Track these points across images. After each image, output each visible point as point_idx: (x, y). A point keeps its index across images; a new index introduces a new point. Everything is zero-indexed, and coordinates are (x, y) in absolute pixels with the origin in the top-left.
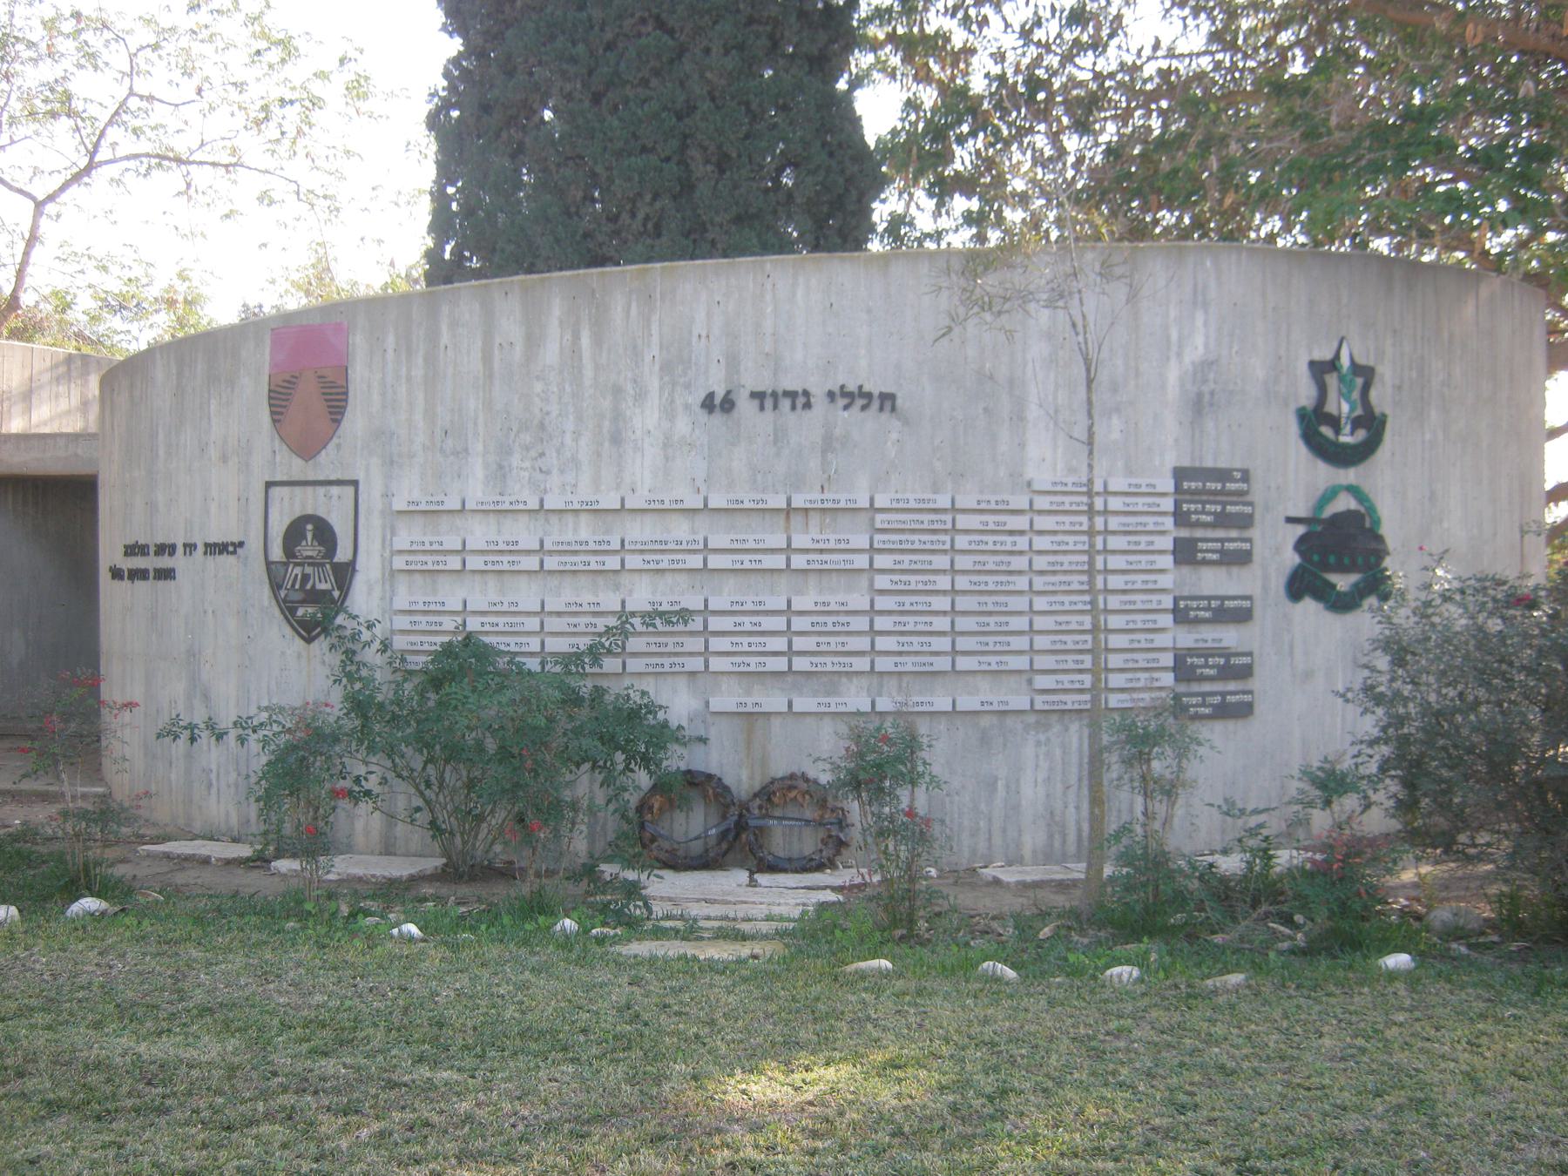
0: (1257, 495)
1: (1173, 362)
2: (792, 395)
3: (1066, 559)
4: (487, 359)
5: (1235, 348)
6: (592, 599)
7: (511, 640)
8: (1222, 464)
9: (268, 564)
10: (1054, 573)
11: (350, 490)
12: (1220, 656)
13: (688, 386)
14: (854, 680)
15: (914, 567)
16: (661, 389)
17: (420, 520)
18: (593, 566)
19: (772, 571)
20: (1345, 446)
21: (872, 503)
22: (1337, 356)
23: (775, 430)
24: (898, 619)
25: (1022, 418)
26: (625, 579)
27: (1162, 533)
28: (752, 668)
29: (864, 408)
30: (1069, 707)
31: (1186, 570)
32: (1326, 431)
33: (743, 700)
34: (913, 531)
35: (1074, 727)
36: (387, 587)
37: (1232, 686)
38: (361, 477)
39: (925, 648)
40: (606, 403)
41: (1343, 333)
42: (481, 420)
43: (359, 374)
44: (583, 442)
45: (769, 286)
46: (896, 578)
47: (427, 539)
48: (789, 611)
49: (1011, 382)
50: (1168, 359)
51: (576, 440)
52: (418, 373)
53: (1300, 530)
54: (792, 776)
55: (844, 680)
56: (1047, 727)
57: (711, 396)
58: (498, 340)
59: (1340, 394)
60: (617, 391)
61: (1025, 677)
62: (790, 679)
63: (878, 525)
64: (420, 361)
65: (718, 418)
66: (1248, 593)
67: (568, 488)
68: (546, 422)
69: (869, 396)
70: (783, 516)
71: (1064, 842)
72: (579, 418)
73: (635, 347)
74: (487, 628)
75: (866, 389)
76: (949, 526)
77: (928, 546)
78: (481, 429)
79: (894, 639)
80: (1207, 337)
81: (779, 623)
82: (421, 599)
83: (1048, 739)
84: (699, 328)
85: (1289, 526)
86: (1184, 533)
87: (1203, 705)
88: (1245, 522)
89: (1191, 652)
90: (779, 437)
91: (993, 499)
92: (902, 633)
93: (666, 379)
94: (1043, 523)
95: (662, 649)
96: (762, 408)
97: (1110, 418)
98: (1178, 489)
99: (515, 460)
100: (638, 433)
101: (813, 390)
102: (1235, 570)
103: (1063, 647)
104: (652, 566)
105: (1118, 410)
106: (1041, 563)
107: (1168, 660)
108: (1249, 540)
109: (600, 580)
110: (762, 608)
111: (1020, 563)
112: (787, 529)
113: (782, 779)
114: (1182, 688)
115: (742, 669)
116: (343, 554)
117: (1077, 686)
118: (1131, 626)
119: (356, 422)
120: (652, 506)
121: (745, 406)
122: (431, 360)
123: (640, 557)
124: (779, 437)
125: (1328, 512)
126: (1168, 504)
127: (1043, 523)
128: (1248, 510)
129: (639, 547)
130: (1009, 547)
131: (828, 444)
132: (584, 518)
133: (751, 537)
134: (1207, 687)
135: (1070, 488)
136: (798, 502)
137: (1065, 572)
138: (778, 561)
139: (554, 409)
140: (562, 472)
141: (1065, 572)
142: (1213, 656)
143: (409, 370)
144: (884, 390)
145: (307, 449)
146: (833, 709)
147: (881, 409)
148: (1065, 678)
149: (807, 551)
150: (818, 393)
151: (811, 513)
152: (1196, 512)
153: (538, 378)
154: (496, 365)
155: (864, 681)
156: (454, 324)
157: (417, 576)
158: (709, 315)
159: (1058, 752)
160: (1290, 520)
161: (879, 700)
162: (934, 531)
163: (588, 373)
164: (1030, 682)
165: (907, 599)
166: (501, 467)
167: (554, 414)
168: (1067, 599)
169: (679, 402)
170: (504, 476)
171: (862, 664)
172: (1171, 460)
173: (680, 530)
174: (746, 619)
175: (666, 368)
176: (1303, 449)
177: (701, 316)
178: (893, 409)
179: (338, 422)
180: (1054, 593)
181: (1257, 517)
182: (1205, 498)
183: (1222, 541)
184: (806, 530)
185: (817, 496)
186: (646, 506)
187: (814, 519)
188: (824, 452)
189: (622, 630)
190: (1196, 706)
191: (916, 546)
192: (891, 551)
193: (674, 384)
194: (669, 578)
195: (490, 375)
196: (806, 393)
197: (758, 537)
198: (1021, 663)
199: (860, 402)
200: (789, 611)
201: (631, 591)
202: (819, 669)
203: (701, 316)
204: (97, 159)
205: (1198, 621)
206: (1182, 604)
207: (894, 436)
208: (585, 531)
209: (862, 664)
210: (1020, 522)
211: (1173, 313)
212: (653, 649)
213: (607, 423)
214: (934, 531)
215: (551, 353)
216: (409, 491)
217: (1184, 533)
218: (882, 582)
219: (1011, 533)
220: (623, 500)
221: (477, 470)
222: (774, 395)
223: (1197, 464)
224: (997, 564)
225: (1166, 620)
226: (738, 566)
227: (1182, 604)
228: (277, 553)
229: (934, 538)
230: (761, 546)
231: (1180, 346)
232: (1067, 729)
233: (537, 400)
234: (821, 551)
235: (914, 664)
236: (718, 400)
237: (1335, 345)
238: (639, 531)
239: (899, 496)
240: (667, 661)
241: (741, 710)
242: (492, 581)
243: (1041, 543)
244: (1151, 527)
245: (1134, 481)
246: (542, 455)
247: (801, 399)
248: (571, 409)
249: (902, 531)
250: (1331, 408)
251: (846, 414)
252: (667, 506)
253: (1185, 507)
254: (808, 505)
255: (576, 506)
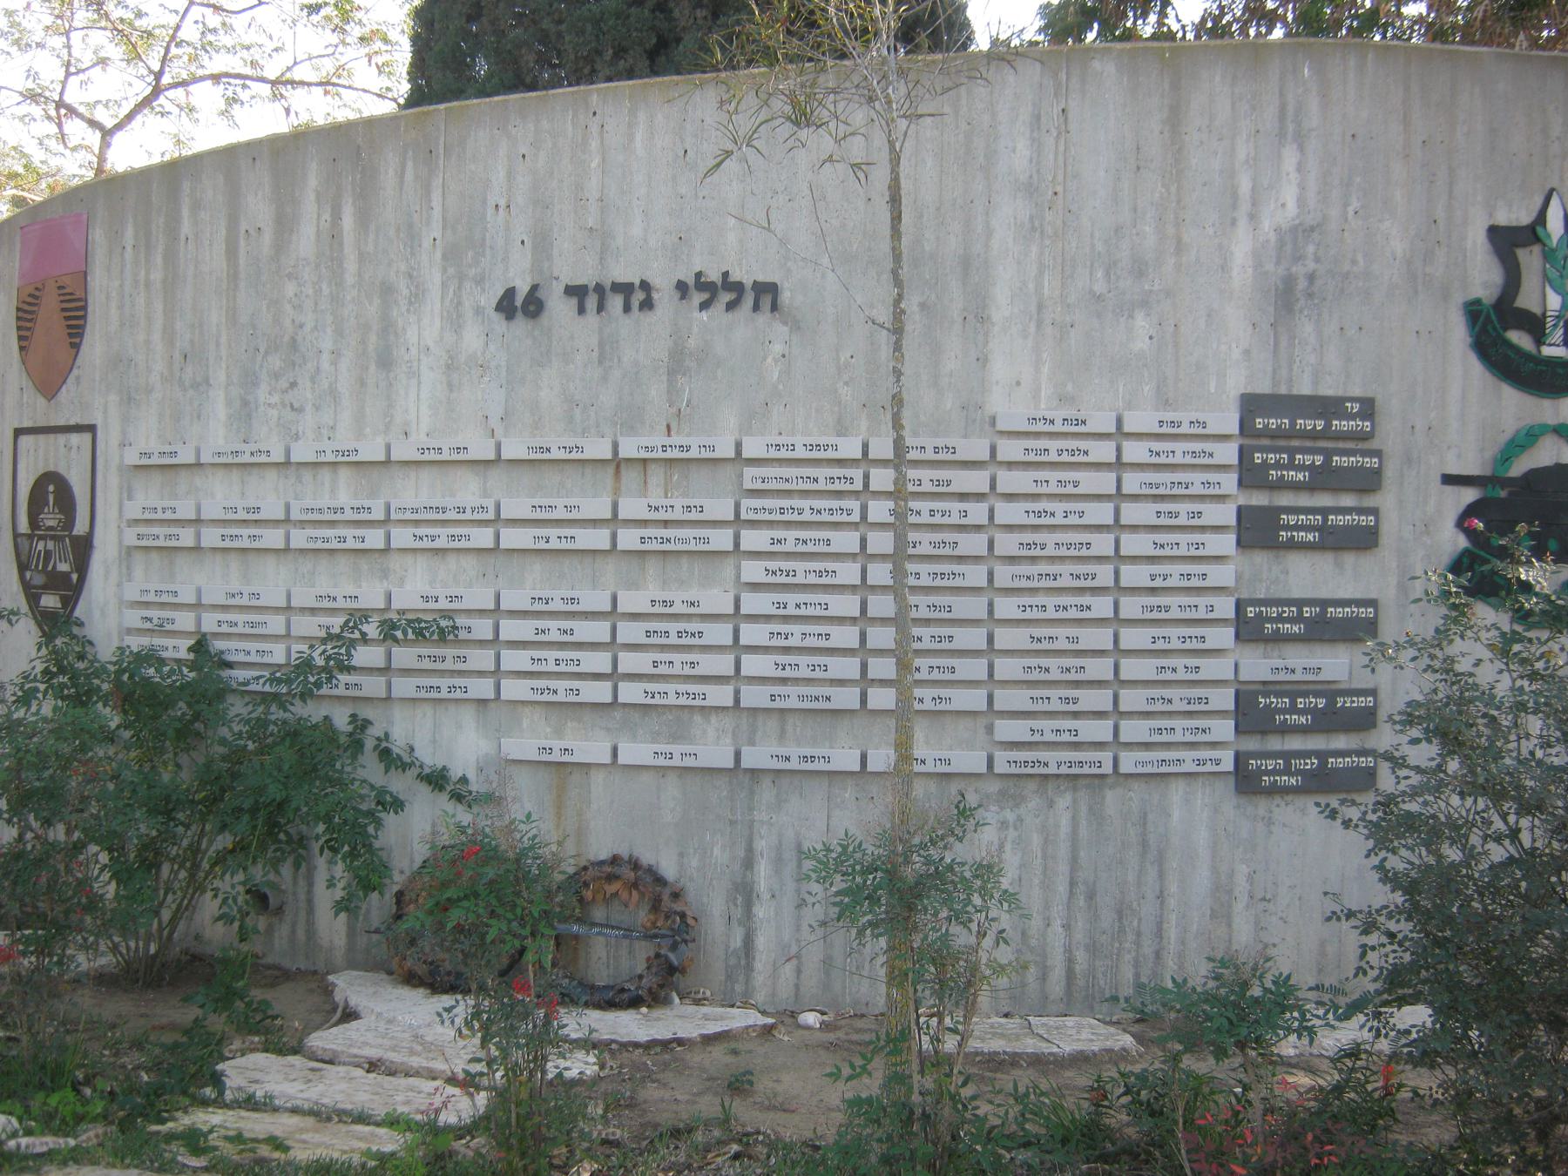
0: (1390, 435)
1: (1243, 228)
2: (625, 289)
3: (1049, 538)
4: (231, 252)
5: (1355, 204)
6: (350, 590)
7: (253, 646)
8: (1328, 389)
9: (16, 535)
10: (1033, 560)
11: (87, 437)
12: (1317, 694)
13: (480, 281)
14: (713, 719)
15: (801, 548)
16: (444, 285)
17: (157, 477)
18: (350, 544)
19: (594, 552)
20: (1553, 362)
21: (738, 451)
22: (1541, 218)
23: (601, 345)
24: (777, 628)
25: (983, 319)
26: (395, 562)
27: (1221, 498)
28: (560, 697)
29: (731, 306)
30: (1052, 770)
31: (1260, 558)
32: (1519, 339)
33: (547, 743)
34: (805, 494)
35: (1064, 802)
36: (124, 571)
37: (1340, 742)
38: (97, 419)
39: (818, 674)
40: (372, 309)
41: (1555, 183)
42: (224, 339)
43: (99, 282)
44: (344, 364)
45: (595, 129)
46: (773, 565)
47: (159, 504)
48: (612, 613)
49: (966, 263)
50: (1234, 222)
51: (334, 363)
52: (157, 276)
53: (1470, 495)
54: (615, 860)
55: (698, 718)
56: (1018, 800)
57: (510, 293)
58: (243, 226)
59: (1546, 278)
60: (387, 290)
61: (982, 722)
62: (618, 714)
63: (748, 485)
64: (159, 260)
65: (521, 324)
66: (1373, 596)
67: (325, 432)
68: (299, 338)
69: (738, 288)
70: (611, 470)
71: (1043, 978)
72: (339, 332)
73: (410, 226)
74: (225, 629)
75: (736, 276)
76: (858, 486)
77: (825, 517)
78: (224, 353)
79: (770, 659)
80: (1302, 187)
81: (598, 631)
82: (152, 587)
83: (1020, 819)
84: (496, 196)
85: (1449, 489)
86: (1259, 499)
87: (1287, 771)
88: (1369, 482)
89: (1267, 687)
90: (606, 352)
91: (930, 443)
92: (787, 650)
93: (451, 271)
94: (1010, 481)
95: (439, 666)
96: (581, 310)
97: (1131, 317)
98: (1245, 427)
99: (262, 394)
100: (414, 351)
101: (655, 281)
102: (1349, 558)
103: (1044, 676)
104: (426, 544)
105: (1145, 303)
106: (1007, 544)
107: (1224, 699)
108: (1374, 512)
109: (364, 564)
110: (574, 608)
111: (974, 544)
112: (617, 491)
113: (602, 863)
114: (1251, 744)
115: (546, 697)
116: (80, 528)
117: (1066, 737)
118: (1160, 645)
119: (95, 347)
120: (427, 457)
121: (559, 307)
122: (170, 257)
123: (411, 530)
124: (606, 352)
125: (1518, 469)
126: (1228, 453)
127: (1010, 481)
128: (1371, 462)
129: (408, 516)
130: (955, 519)
131: (677, 364)
132: (344, 474)
133: (560, 502)
134: (1295, 743)
135: (1058, 427)
136: (629, 449)
137: (1052, 559)
138: (598, 539)
139: (309, 319)
140: (317, 408)
141: (1052, 559)
142: (1305, 694)
143: (148, 273)
144: (761, 278)
145: (49, 382)
146: (676, 762)
147: (756, 307)
148: (1047, 725)
149: (644, 523)
150: (663, 284)
151: (652, 467)
152: (1278, 465)
153: (289, 276)
154: (242, 260)
155: (728, 721)
156: (196, 206)
157: (154, 555)
158: (510, 176)
159: (1036, 840)
160: (1449, 480)
161: (746, 751)
162: (839, 494)
163: (351, 266)
164: (990, 729)
165: (792, 598)
166: (245, 403)
167: (308, 328)
168: (1051, 601)
169: (468, 305)
170: (249, 416)
171: (721, 695)
172: (1237, 383)
173: (468, 492)
174: (553, 624)
175: (451, 255)
176: (1476, 366)
177: (499, 176)
178: (774, 307)
179: (76, 347)
180: (1033, 591)
181: (1390, 473)
182: (1295, 443)
183: (1325, 512)
184: (644, 490)
185: (659, 440)
186: (418, 457)
187: (656, 476)
188: (672, 373)
189: (343, 640)
190: (1274, 772)
191: (807, 516)
192: (771, 524)
193: (461, 278)
194: (452, 560)
195: (234, 276)
196: (645, 286)
197: (571, 501)
198: (974, 699)
199: (726, 297)
200: (612, 613)
201: (402, 581)
202: (657, 701)
203: (499, 176)
204: (166, 80)
205: (1278, 639)
206: (1251, 612)
207: (778, 348)
208: (343, 494)
209: (721, 695)
210: (976, 481)
211: (1242, 152)
212: (427, 664)
213: (373, 338)
214: (839, 494)
215: (306, 240)
216: (147, 438)
217: (1259, 499)
218: (753, 571)
219: (963, 497)
220: (388, 448)
221: (219, 408)
222: (599, 289)
223: (1283, 390)
224: (935, 545)
225: (1223, 637)
226: (542, 545)
227: (1251, 612)
228: (24, 526)
229: (786, 503)
230: (574, 515)
231: (1255, 203)
232: (1051, 804)
233: (288, 307)
234: (666, 524)
235: (801, 697)
236: (519, 301)
237: (1538, 201)
238: (412, 493)
239: (780, 440)
240: (444, 683)
241: (545, 757)
242: (234, 563)
243: (1009, 513)
244: (1196, 489)
245: (1169, 416)
246: (293, 385)
247: (637, 295)
248: (329, 319)
249: (788, 493)
250: (1527, 300)
251: (704, 315)
252: (445, 456)
253: (1258, 458)
254: (644, 455)
255: (330, 458)
